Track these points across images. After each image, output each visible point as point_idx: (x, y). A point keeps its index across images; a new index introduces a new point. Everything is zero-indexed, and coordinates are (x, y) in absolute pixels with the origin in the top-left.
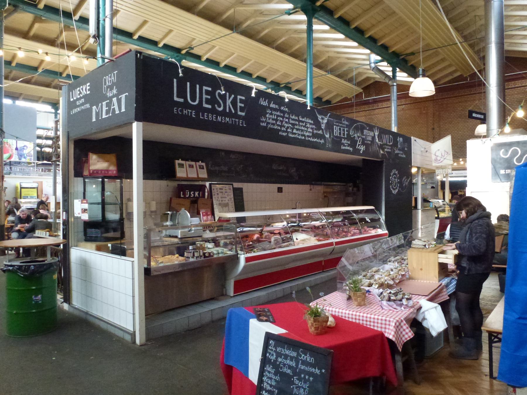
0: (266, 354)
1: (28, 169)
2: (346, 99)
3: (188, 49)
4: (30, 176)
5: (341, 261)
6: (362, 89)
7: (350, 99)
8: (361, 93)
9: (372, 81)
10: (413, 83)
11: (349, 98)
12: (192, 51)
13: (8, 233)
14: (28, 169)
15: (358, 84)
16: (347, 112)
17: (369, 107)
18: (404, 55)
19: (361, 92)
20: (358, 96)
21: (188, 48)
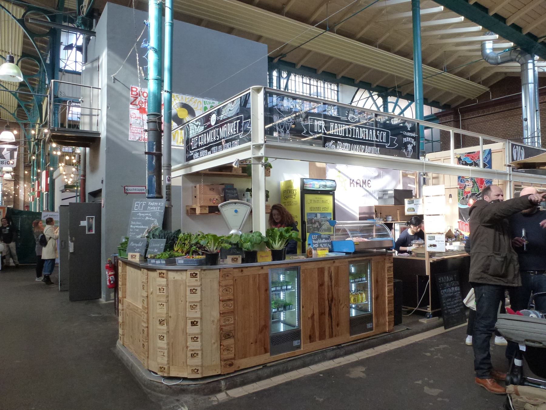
0: (67, 155)
1: (380, 137)
2: (469, 101)
3: (280, 57)
4: (364, 151)
5: (468, 232)
6: (489, 87)
7: (474, 101)
8: (488, 93)
9: (500, 78)
10: (102, 190)
11: (472, 99)
12: (283, 59)
13: (522, 237)
14: (380, 137)
15: (484, 83)
16: (488, 113)
17: (446, 120)
18: (391, 88)
19: (488, 91)
20: (485, 95)
21: (279, 56)
